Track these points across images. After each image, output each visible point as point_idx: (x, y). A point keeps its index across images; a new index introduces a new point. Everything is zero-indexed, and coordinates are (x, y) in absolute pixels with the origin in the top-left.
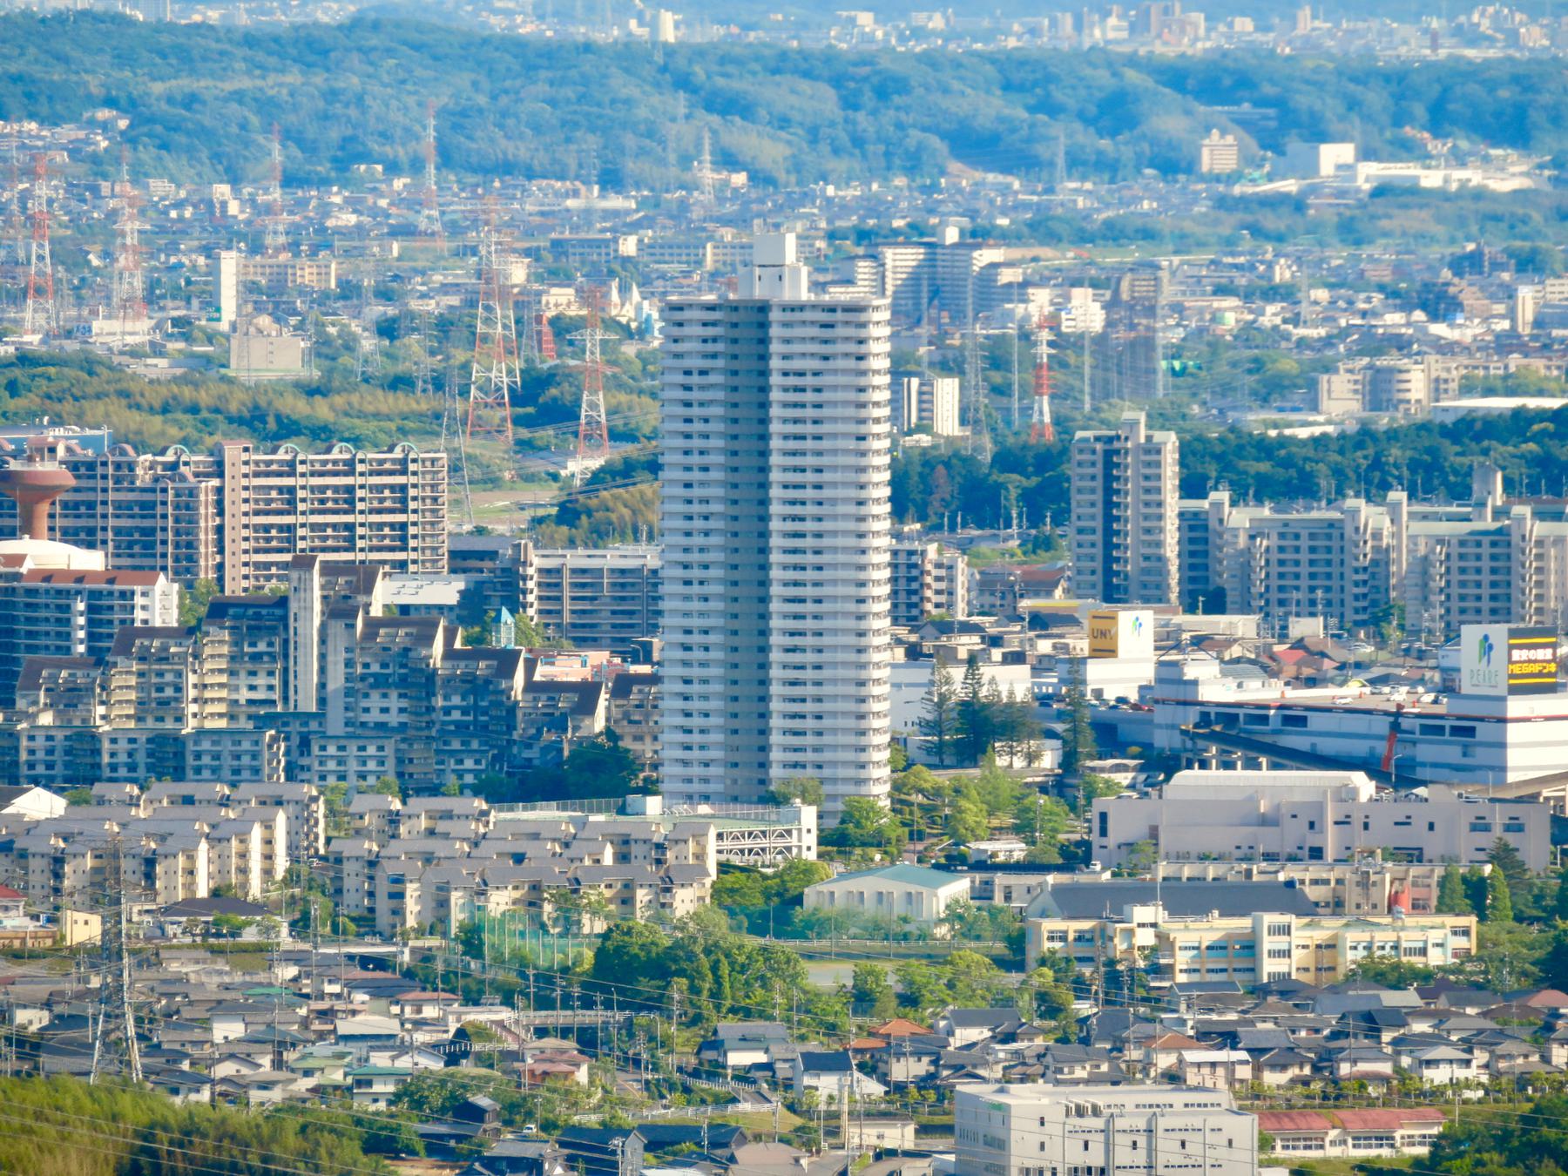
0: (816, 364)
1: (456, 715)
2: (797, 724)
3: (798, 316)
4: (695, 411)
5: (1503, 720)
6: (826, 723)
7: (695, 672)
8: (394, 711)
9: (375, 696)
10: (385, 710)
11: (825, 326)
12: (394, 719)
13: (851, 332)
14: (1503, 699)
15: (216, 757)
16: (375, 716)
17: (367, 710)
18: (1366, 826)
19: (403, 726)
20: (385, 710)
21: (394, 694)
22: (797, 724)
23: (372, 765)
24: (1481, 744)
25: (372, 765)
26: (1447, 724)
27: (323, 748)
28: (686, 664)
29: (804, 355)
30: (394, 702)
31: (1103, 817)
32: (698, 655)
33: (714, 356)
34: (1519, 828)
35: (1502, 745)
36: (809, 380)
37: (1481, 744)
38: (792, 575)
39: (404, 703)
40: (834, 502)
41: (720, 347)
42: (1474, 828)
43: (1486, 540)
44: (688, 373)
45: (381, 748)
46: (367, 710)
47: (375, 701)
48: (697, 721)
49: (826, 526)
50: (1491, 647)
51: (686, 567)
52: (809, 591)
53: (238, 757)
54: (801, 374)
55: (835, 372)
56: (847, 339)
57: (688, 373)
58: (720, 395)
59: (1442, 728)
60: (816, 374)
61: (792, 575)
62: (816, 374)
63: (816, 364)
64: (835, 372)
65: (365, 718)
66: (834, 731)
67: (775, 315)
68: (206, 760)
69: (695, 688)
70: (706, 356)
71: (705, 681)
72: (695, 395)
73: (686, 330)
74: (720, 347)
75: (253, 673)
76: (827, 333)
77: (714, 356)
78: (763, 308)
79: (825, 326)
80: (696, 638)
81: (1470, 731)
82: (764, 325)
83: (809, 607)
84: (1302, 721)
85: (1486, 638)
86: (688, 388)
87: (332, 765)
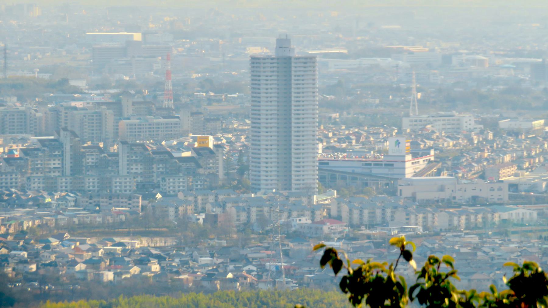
1: (161, 170)
2: (298, 169)
3: (298, 61)
4: (269, 86)
5: (404, 162)
6: (305, 168)
7: (269, 156)
9: (134, 165)
11: (305, 63)
12: (139, 171)
13: (311, 64)
14: (404, 156)
15: (120, 183)
16: (134, 171)
18: (465, 191)
19: (141, 173)
21: (139, 165)
22: (298, 169)
23: (181, 184)
26: (383, 163)
28: (267, 154)
30: (139, 167)
32: (269, 151)
33: (273, 72)
34: (501, 190)
35: (404, 168)
38: (296, 129)
39: (141, 167)
40: (307, 110)
41: (275, 69)
42: (491, 190)
43: (95, 115)
44: (267, 76)
45: (184, 179)
47: (134, 167)
48: (269, 169)
49: (305, 116)
53: (89, 183)
55: (307, 75)
56: (310, 66)
57: (267, 76)
58: (276, 82)
59: (382, 165)
60: (302, 76)
61: (296, 129)
62: (302, 76)
66: (307, 171)
67: (293, 60)
68: (118, 184)
69: (269, 160)
71: (271, 158)
72: (269, 82)
74: (275, 69)
75: (54, 160)
76: (305, 65)
77: (273, 72)
78: (290, 58)
79: (305, 63)
80: (269, 147)
81: (392, 165)
83: (301, 138)
84: (328, 164)
85: (398, 140)
86: (267, 80)
87: (171, 184)
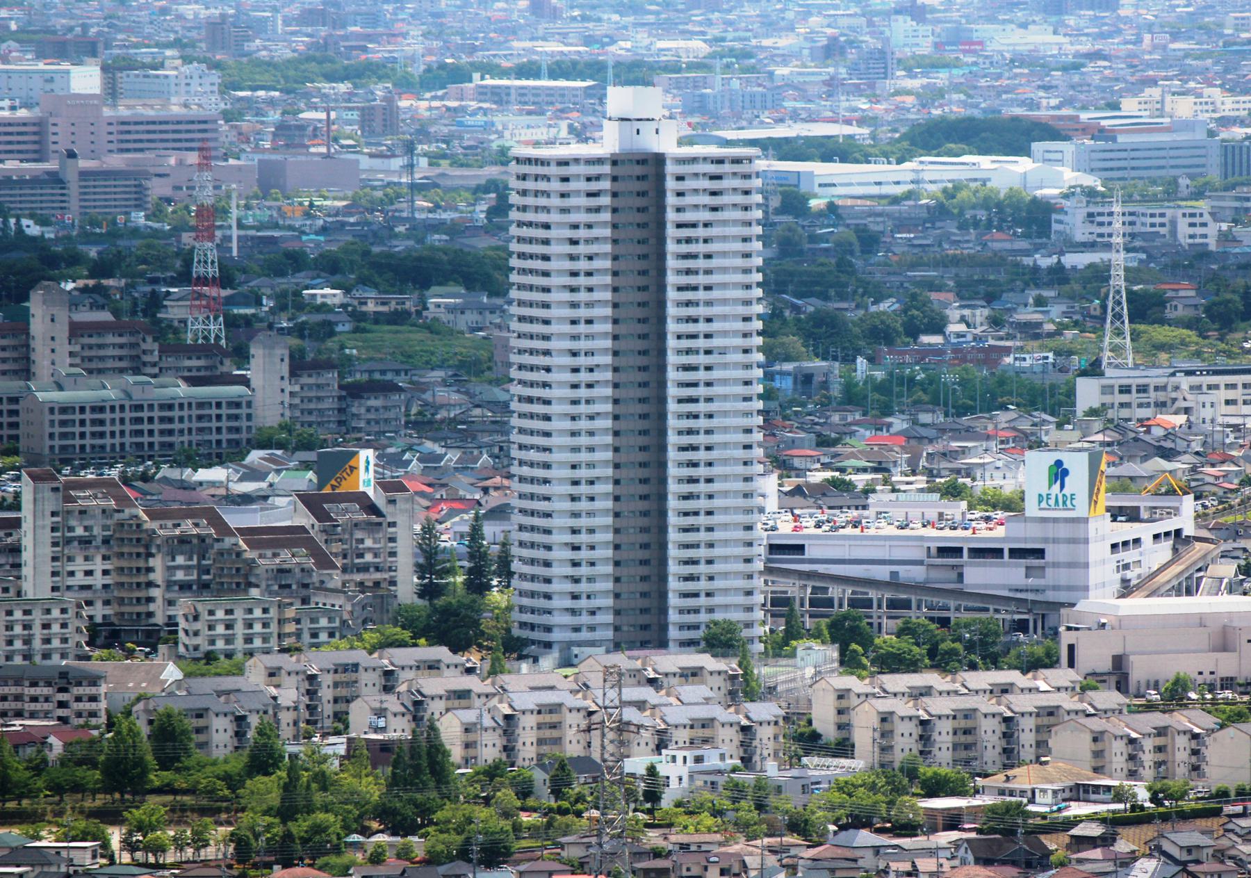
0: (706, 216)
8: (98, 574)
10: (89, 573)
17: (72, 574)
20: (89, 573)
24: (1056, 565)
25: (258, 628)
27: (211, 613)
29: (696, 206)
31: (1071, 648)
33: (598, 210)
36: (701, 232)
37: (1056, 565)
46: (72, 574)
47: (79, 565)
50: (1065, 473)
51: (573, 419)
52: (701, 439)
53: (250, 626)
54: (694, 225)
55: (724, 223)
63: (706, 216)
64: (724, 223)
65: (70, 581)
67: (670, 168)
70: (589, 210)
73: (572, 186)
76: (715, 185)
77: (598, 210)
82: (661, 178)
